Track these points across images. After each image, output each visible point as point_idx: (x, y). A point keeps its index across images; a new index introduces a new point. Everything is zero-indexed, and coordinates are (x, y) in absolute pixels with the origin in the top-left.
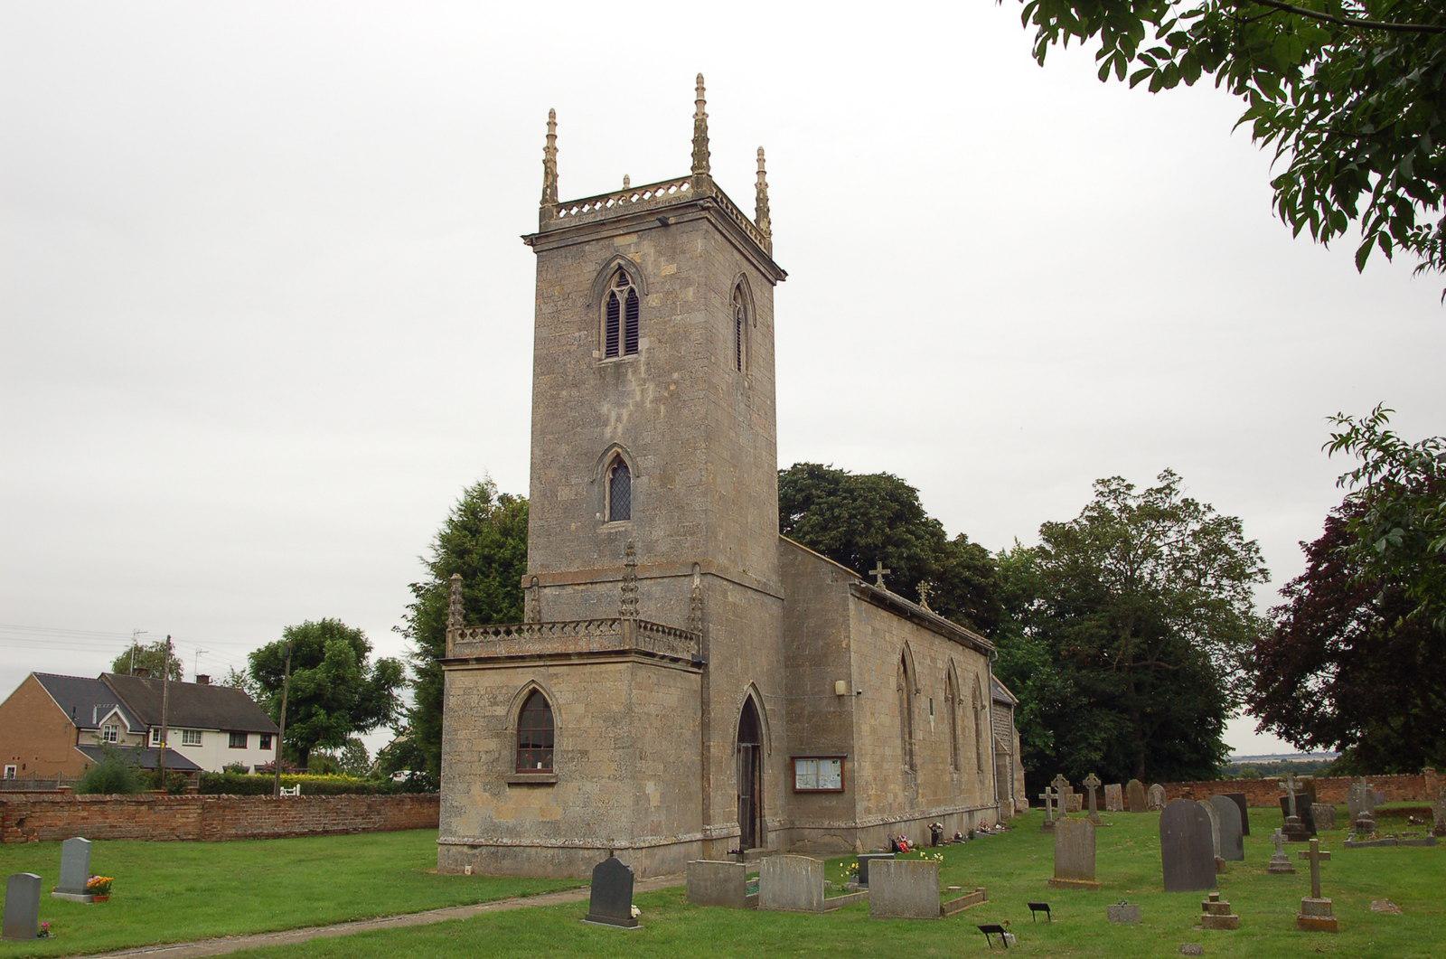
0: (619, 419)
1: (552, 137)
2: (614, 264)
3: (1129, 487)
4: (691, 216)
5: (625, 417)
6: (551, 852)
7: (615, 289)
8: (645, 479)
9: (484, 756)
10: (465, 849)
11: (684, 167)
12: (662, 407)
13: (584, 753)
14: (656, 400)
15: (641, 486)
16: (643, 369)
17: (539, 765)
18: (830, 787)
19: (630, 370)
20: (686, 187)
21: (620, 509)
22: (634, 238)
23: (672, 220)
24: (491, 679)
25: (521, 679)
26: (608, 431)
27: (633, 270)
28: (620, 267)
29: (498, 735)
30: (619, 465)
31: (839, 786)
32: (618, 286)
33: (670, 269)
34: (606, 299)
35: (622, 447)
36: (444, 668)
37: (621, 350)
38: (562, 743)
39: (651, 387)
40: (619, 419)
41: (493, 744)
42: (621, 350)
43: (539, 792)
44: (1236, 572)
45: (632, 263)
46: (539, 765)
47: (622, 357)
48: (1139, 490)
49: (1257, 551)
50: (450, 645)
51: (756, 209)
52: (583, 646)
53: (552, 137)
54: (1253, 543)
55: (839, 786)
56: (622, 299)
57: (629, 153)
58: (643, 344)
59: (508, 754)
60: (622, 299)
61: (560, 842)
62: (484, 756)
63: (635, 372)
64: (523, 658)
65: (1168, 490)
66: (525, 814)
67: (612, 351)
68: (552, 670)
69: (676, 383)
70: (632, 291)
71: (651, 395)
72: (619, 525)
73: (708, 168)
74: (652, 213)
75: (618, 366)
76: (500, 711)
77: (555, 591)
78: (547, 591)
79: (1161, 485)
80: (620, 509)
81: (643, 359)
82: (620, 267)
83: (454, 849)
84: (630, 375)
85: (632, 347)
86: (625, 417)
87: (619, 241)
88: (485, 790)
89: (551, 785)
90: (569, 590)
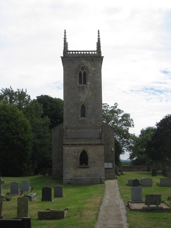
0: (83, 97)
1: (65, 36)
2: (81, 66)
3: (108, 106)
4: (98, 59)
5: (85, 97)
6: (88, 180)
7: (81, 71)
8: (89, 110)
9: (73, 163)
10: (69, 180)
11: (95, 49)
12: (93, 96)
13: (95, 162)
14: (91, 95)
15: (88, 111)
16: (88, 88)
17: (84, 164)
18: (111, 167)
19: (86, 88)
20: (96, 53)
21: (83, 115)
22: (86, 61)
23: (94, 59)
24: (74, 148)
25: (81, 148)
26: (81, 100)
27: (86, 68)
28: (82, 66)
29: (76, 159)
30: (83, 107)
31: (112, 167)
32: (81, 70)
33: (94, 69)
34: (79, 72)
35: (84, 103)
36: (63, 146)
37: (83, 84)
38: (90, 160)
39: (90, 92)
40: (83, 97)
41: (75, 160)
42: (83, 84)
43: (85, 169)
44: (128, 124)
45: (85, 66)
46: (84, 164)
47: (82, 85)
48: (110, 106)
49: (133, 121)
50: (64, 141)
51: (64, 41)
52: (94, 142)
53: (65, 36)
54: (132, 119)
55: (112, 167)
56: (82, 73)
57: (82, 44)
58: (88, 83)
59: (79, 162)
60: (82, 73)
61: (90, 178)
62: (73, 163)
63: (87, 89)
64: (81, 144)
65: (116, 107)
66: (83, 173)
67: (80, 82)
68: (88, 147)
69: (96, 92)
70: (85, 72)
71: (90, 94)
72: (83, 118)
73: (100, 50)
74: (90, 57)
75: (83, 87)
76: (76, 154)
77: (70, 130)
78: (68, 130)
79: (114, 106)
80: (83, 115)
81: (88, 86)
82: (82, 66)
83: (67, 180)
84: (86, 89)
85: (85, 83)
86: (85, 97)
87: (82, 61)
88: (74, 169)
89: (88, 168)
90: (73, 130)
